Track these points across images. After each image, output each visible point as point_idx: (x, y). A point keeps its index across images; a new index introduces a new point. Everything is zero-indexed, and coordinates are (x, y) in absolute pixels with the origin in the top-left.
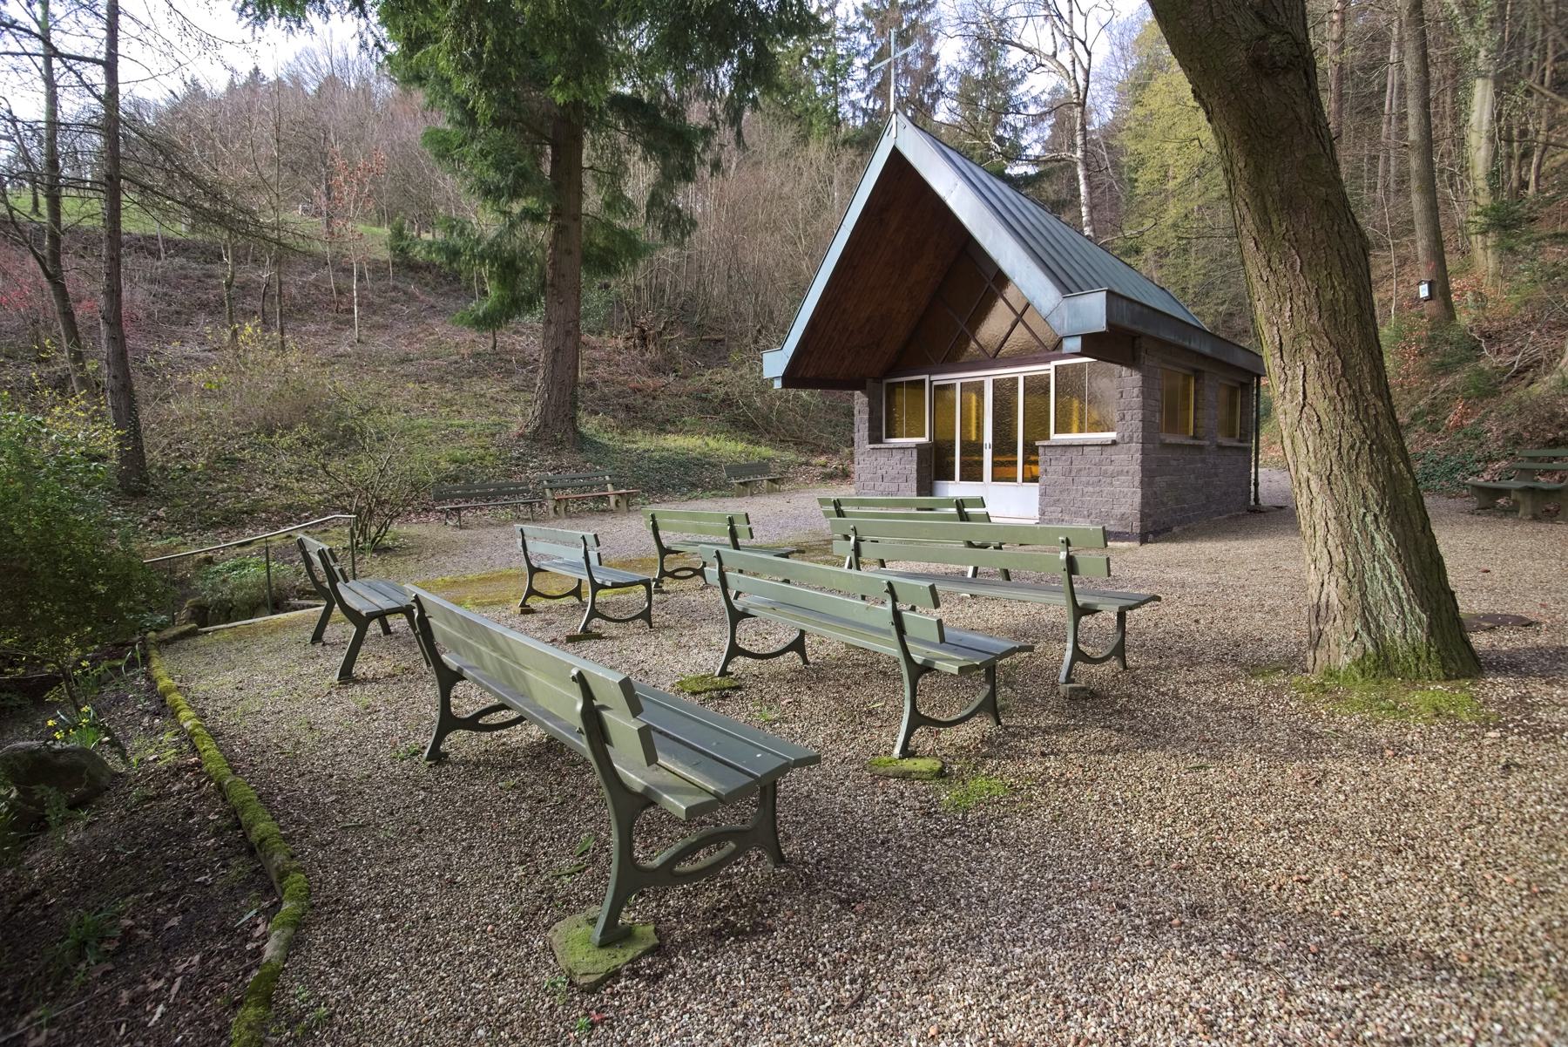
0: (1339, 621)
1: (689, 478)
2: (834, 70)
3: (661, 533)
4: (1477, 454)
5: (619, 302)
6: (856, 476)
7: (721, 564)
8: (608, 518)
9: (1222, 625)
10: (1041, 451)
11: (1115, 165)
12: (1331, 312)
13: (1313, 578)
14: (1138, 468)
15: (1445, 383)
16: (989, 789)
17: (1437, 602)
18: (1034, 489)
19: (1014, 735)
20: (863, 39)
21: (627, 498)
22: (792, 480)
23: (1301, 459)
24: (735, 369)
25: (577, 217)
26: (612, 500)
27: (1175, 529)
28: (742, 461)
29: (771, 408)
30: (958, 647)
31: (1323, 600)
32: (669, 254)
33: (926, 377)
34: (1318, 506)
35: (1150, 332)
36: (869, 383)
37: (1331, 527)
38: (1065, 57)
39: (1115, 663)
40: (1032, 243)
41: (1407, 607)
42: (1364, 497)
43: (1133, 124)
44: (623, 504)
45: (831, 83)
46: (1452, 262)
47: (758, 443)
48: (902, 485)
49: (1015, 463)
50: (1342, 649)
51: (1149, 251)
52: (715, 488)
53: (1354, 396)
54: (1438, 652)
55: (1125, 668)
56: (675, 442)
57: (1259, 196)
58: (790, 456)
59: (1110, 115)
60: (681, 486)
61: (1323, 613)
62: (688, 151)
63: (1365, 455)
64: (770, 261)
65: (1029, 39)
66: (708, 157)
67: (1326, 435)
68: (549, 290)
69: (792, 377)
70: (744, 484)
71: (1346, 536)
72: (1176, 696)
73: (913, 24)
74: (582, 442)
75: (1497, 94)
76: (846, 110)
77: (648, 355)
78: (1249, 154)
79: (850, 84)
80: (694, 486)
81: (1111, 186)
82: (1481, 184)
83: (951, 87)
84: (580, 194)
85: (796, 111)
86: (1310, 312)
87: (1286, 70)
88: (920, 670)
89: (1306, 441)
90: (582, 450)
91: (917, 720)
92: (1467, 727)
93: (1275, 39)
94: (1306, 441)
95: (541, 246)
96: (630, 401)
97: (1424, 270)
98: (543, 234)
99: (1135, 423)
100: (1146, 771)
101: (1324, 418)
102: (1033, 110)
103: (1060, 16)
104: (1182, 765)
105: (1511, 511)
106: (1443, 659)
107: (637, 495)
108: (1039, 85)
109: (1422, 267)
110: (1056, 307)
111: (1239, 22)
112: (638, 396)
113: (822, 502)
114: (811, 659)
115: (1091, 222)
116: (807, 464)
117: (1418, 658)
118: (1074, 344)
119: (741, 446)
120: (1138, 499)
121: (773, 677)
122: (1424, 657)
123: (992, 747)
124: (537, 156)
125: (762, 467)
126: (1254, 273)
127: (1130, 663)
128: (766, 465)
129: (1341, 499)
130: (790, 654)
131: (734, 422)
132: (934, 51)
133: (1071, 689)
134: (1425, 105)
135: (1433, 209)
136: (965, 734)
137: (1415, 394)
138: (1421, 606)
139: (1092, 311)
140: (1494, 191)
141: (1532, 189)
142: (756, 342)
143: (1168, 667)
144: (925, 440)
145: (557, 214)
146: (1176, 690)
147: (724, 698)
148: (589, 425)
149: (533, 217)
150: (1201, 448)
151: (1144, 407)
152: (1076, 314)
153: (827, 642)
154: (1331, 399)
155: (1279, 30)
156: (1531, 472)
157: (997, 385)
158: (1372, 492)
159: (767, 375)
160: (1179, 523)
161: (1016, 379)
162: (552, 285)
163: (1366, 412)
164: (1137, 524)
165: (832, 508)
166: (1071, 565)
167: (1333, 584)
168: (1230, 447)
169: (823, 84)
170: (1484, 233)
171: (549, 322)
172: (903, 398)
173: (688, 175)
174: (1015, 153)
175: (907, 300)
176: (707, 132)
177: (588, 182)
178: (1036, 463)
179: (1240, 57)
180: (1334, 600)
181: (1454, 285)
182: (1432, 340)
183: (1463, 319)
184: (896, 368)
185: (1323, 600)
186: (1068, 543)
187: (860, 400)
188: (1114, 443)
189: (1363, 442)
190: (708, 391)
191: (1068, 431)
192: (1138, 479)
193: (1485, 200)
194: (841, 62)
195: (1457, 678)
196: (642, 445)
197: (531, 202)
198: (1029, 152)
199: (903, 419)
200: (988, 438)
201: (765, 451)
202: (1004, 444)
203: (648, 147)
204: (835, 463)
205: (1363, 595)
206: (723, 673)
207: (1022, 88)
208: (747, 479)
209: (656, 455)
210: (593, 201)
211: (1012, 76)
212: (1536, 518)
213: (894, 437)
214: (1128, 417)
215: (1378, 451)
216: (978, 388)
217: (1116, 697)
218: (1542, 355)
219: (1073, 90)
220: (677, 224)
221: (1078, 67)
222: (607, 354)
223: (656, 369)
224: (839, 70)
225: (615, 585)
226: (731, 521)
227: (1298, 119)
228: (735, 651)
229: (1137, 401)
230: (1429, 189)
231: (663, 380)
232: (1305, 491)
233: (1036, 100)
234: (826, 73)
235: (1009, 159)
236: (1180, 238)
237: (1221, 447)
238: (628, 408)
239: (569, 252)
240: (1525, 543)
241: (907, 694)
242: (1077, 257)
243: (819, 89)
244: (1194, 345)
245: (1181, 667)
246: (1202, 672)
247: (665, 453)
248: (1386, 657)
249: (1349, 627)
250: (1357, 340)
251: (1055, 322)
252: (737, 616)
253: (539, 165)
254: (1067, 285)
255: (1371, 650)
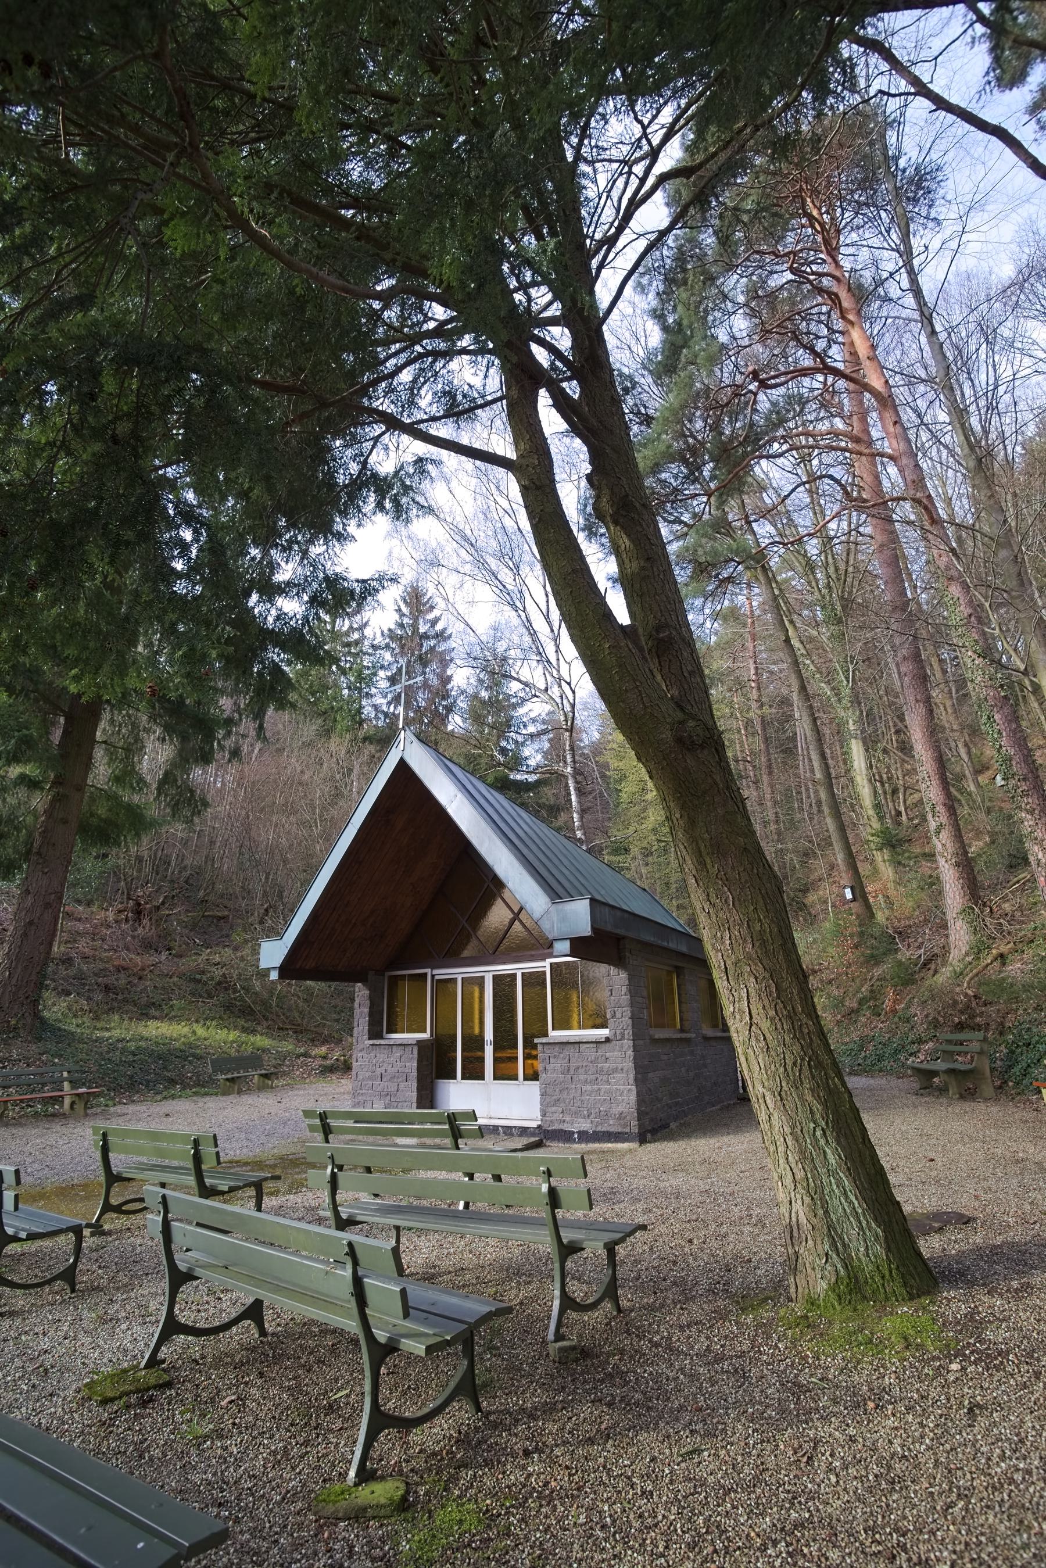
0: (810, 1242)
1: (169, 1073)
2: (360, 678)
3: (112, 1156)
4: (911, 1037)
5: (116, 872)
6: (354, 1073)
7: (166, 1211)
8: (57, 1127)
9: (715, 1244)
10: (540, 1048)
11: (603, 776)
12: (761, 941)
13: (781, 1196)
14: (631, 1065)
15: (877, 972)
16: (461, 1522)
17: (888, 1213)
18: (534, 1087)
19: (495, 1426)
20: (388, 656)
21: (86, 1100)
22: (285, 1074)
23: (755, 1075)
24: (236, 949)
25: (80, 788)
26: (67, 1101)
27: (673, 1125)
28: (233, 1053)
29: (271, 993)
30: (432, 1315)
31: (794, 1219)
32: (178, 829)
33: (428, 971)
34: (775, 1121)
35: (631, 934)
36: (371, 975)
37: (789, 1143)
38: (555, 692)
39: (608, 1305)
40: (525, 851)
41: (864, 1223)
42: (812, 1112)
43: (615, 746)
44: (79, 1107)
45: (356, 688)
46: (864, 869)
47: (254, 1032)
48: (402, 1085)
49: (516, 1058)
50: (817, 1280)
51: (635, 850)
52: (198, 1084)
53: (789, 1017)
54: (897, 1268)
55: (619, 1310)
56: (157, 1030)
57: (693, 840)
58: (287, 1046)
59: (597, 735)
60: (156, 1083)
61: (795, 1234)
62: (210, 737)
63: (806, 1072)
64: (283, 841)
65: (525, 674)
66: (227, 743)
67: (773, 1053)
68: (34, 858)
69: (287, 969)
70: (232, 1080)
71: (802, 1151)
72: (670, 1348)
73: (432, 649)
74: (41, 1029)
75: (867, 750)
76: (368, 711)
77: (140, 930)
78: (682, 808)
79: (373, 691)
80: (172, 1082)
81: (601, 793)
82: (871, 812)
83: (462, 704)
84: (88, 763)
85: (323, 707)
86: (745, 941)
87: (702, 747)
88: (383, 1352)
89: (757, 1058)
90: (40, 1039)
91: (380, 1420)
92: (934, 1359)
93: (691, 723)
94: (757, 1058)
95: (35, 813)
96: (111, 980)
97: (845, 879)
98: (39, 801)
99: (627, 1021)
100: (638, 1467)
101: (768, 1035)
102: (531, 729)
103: (548, 661)
104: (675, 1450)
105: (943, 1090)
106: (903, 1277)
107: (96, 1095)
108: (535, 710)
109: (843, 874)
110: (547, 912)
111: (664, 709)
112: (122, 975)
113: (307, 1114)
114: (269, 1327)
115: (582, 827)
116: (306, 1055)
117: (883, 1277)
118: (564, 946)
119: (233, 1035)
120: (633, 1097)
121: (218, 1362)
122: (887, 1276)
123: (473, 1449)
124: (47, 726)
125: (253, 1060)
126: (698, 906)
127: (624, 1303)
128: (259, 1058)
129: (793, 1115)
130: (246, 1323)
131: (228, 1007)
132: (449, 672)
133: (561, 1349)
134: (823, 756)
135: (842, 829)
136: (442, 1428)
137: (858, 981)
138: (876, 1220)
139: (578, 916)
140: (881, 818)
141: (904, 818)
142: (261, 922)
143: (662, 1306)
144: (425, 1036)
145: (57, 782)
146: (669, 1338)
147: (144, 1404)
148: (55, 1008)
149: (32, 784)
150: (688, 1041)
151: (632, 1004)
152: (564, 919)
153: (284, 1309)
154: (772, 1019)
155: (693, 717)
156: (951, 1053)
157: (496, 978)
158: (817, 1107)
159: (263, 965)
160: (676, 1119)
161: (515, 975)
162: (39, 854)
163: (801, 1032)
164: (635, 1123)
165: (317, 1122)
166: (554, 1198)
167: (799, 1202)
168: (716, 1038)
169: (349, 688)
170: (881, 849)
171: (27, 892)
172: (405, 990)
173: (206, 758)
174: (517, 762)
175: (406, 906)
176: (229, 722)
177: (99, 754)
178: (535, 1057)
179: (667, 735)
180: (803, 1220)
181: (869, 889)
182: (861, 934)
183: (880, 917)
184: (400, 960)
185: (794, 1219)
186: (549, 1173)
187: (361, 992)
188: (608, 1040)
189: (802, 1059)
190: (203, 972)
191: (567, 1026)
192: (632, 1076)
193: (876, 825)
194: (368, 672)
195: (919, 1296)
196: (117, 1033)
197: (29, 769)
198: (529, 762)
199: (405, 1015)
200: (489, 1035)
201: (261, 1041)
202: (504, 1039)
203: (168, 728)
204: (336, 1055)
205: (826, 1212)
206: (153, 1362)
207: (521, 711)
208: (233, 1075)
209: (132, 1046)
210: (101, 771)
211: (513, 700)
212: (962, 1097)
213: (396, 1032)
214: (618, 1015)
215: (816, 1067)
216: (480, 981)
217: (609, 1354)
218: (936, 950)
219: (562, 718)
220: (187, 802)
221: (565, 702)
222: (92, 926)
223: (148, 946)
224: (364, 679)
225: (32, 1237)
226: (196, 1143)
227: (716, 783)
228: (172, 1327)
229: (625, 999)
230: (837, 815)
231: (152, 958)
232: (763, 1106)
233: (534, 721)
234: (352, 679)
235: (511, 770)
236: (659, 841)
237: (706, 1039)
238: (107, 988)
239: (65, 822)
240: (956, 1126)
241: (367, 1387)
242: (566, 862)
243: (346, 692)
244: (672, 945)
245: (675, 1303)
246: (696, 1311)
247: (142, 1044)
248: (857, 1278)
249: (819, 1247)
250: (784, 966)
251: (546, 926)
252: (179, 1278)
253: (48, 733)
254: (556, 892)
255: (842, 1272)
